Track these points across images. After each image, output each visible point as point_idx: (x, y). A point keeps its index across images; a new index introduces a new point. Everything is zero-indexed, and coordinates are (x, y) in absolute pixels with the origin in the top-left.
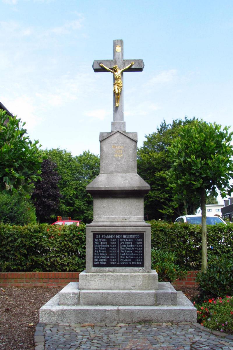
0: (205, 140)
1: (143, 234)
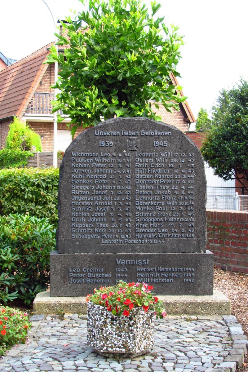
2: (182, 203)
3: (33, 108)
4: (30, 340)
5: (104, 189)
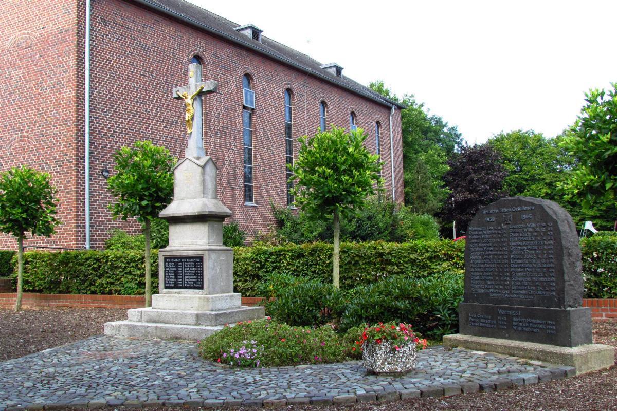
1: (202, 257)
2: (545, 265)
5: (490, 255)
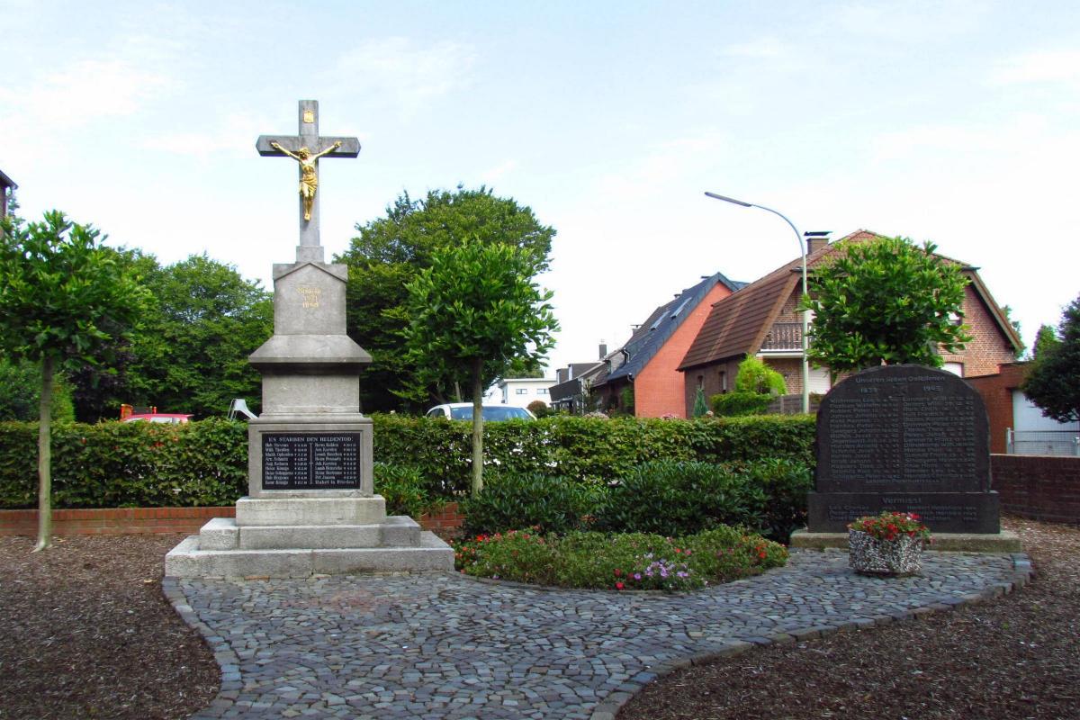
0: (481, 275)
3: (773, 340)
4: (787, 566)
